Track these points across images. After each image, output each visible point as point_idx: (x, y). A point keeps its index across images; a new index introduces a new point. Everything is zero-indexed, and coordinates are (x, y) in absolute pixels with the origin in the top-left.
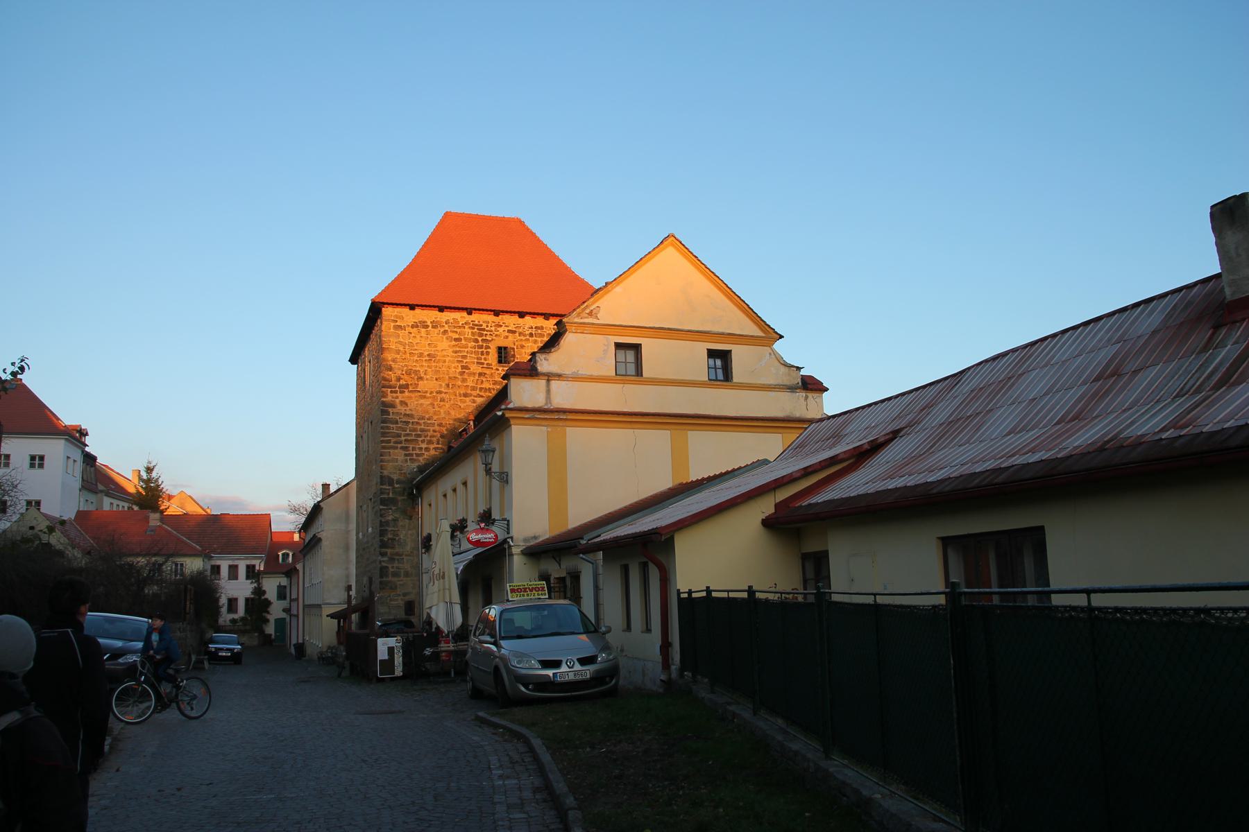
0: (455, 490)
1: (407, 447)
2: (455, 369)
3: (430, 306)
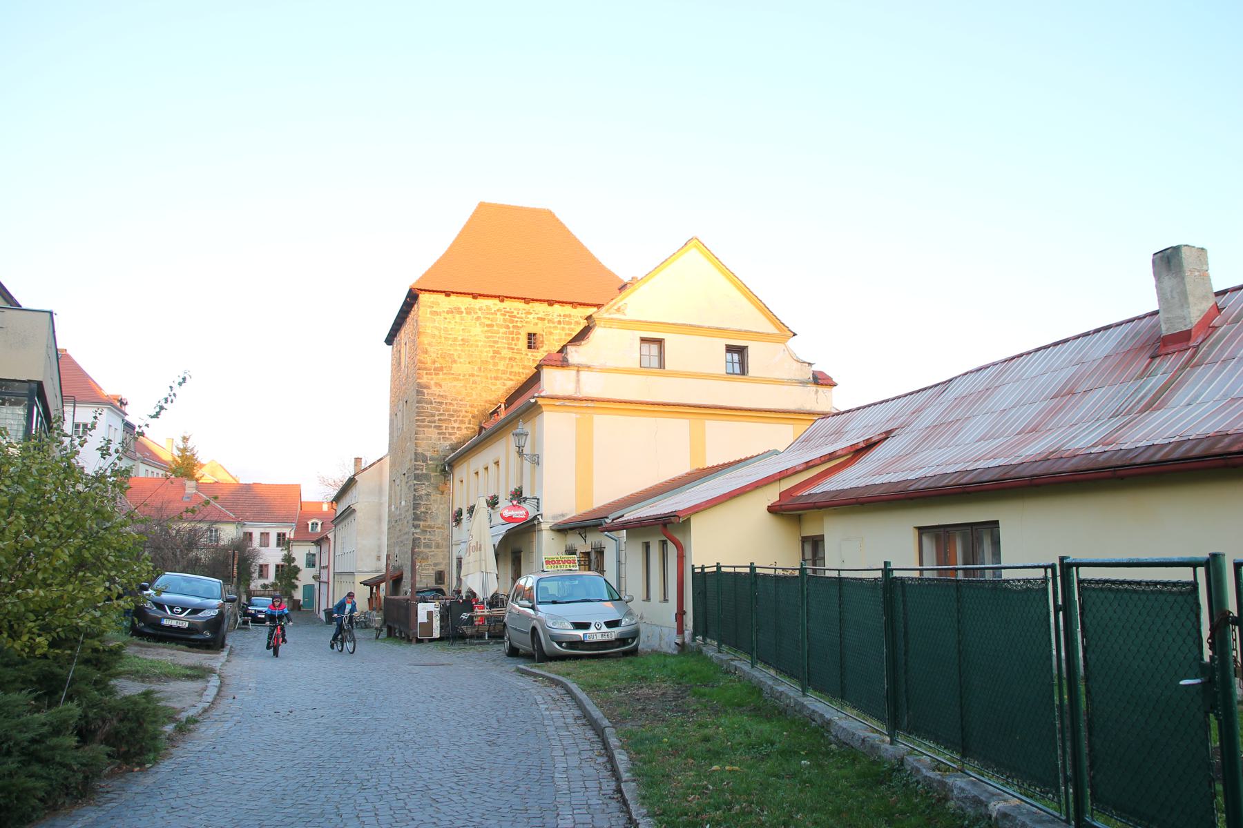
0: (486, 469)
1: (440, 426)
2: (487, 354)
3: (465, 294)
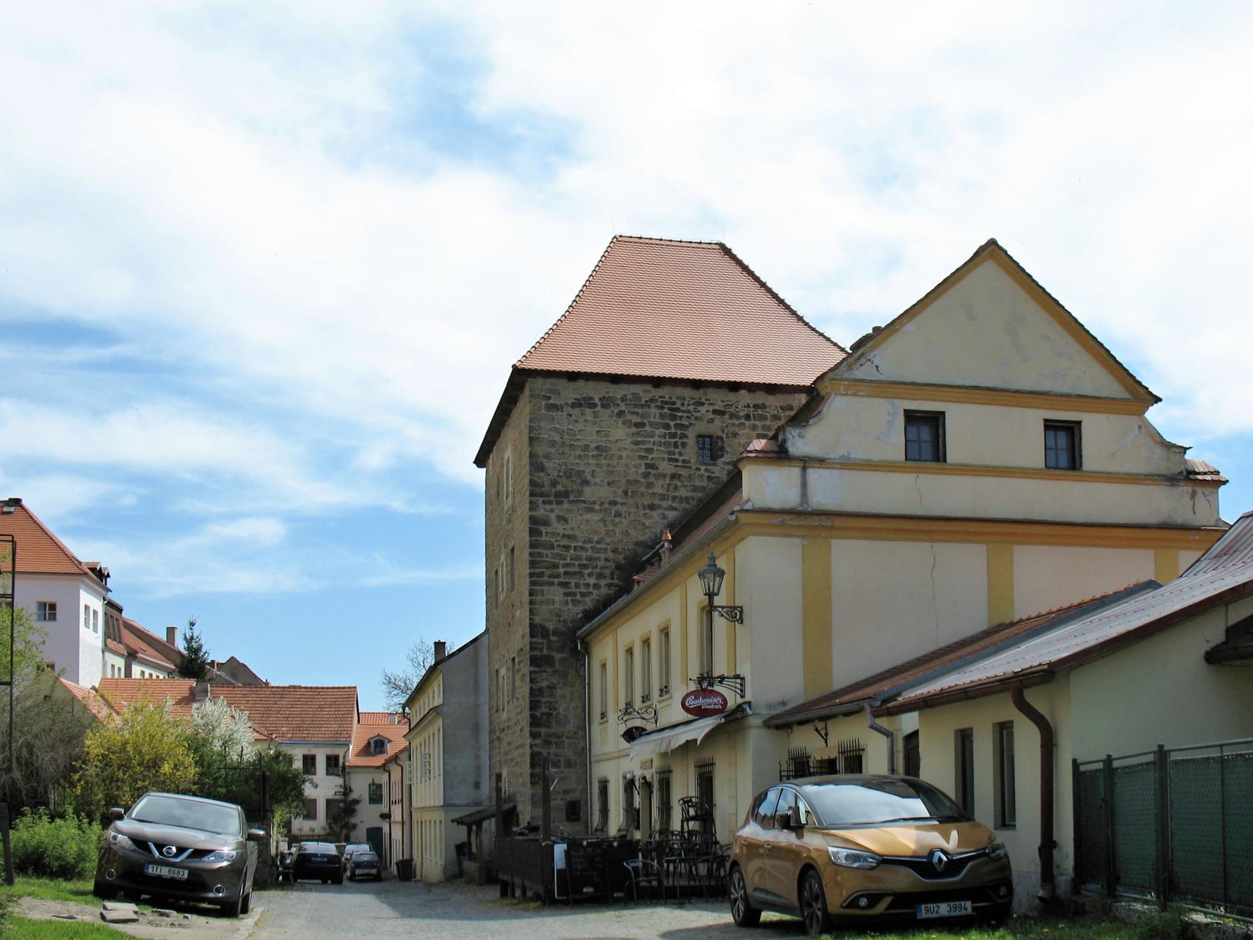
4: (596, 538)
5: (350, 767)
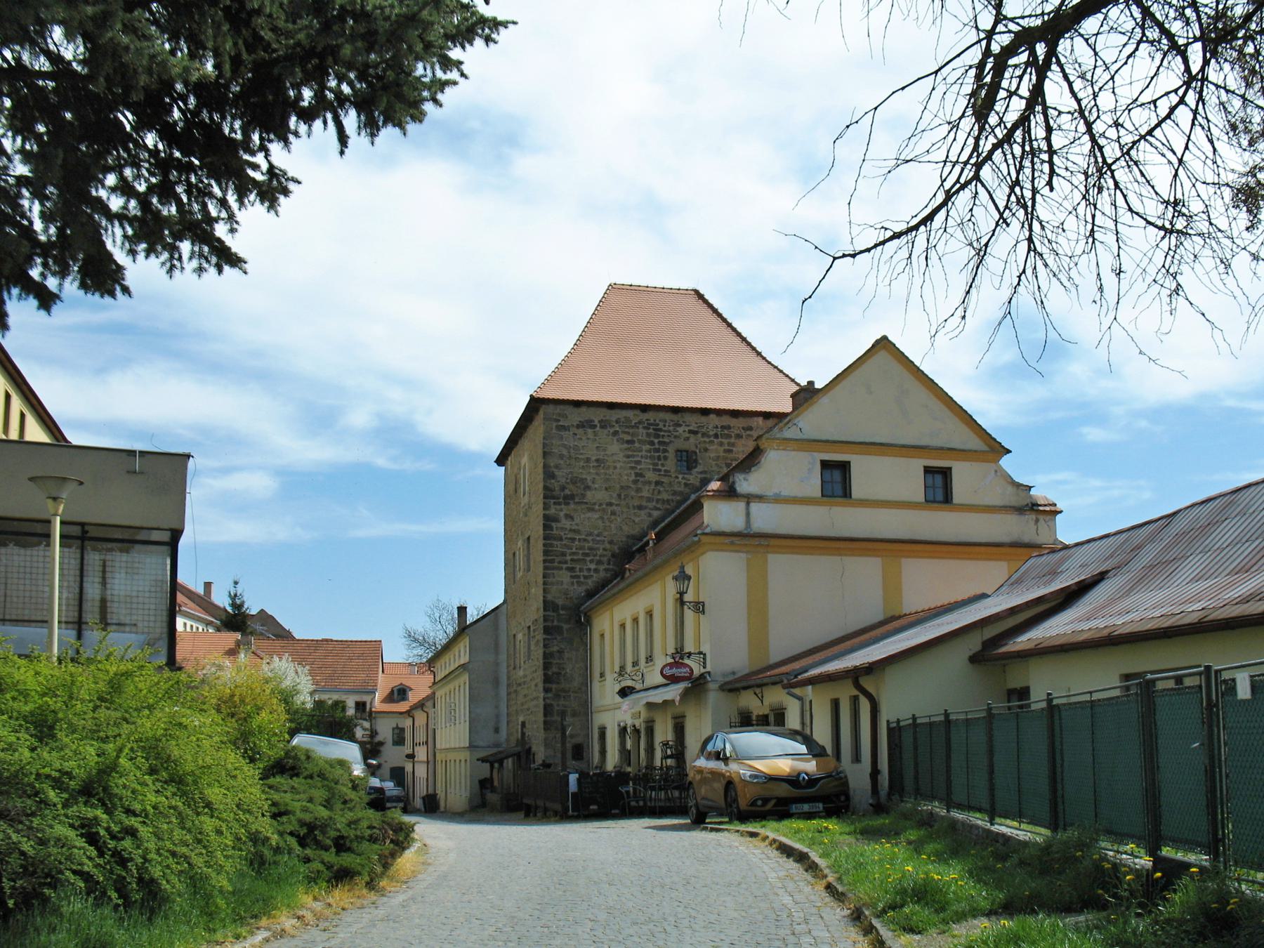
2: (628, 477)
4: (596, 532)
5: (376, 712)
